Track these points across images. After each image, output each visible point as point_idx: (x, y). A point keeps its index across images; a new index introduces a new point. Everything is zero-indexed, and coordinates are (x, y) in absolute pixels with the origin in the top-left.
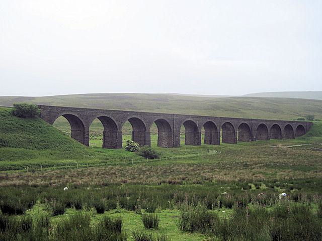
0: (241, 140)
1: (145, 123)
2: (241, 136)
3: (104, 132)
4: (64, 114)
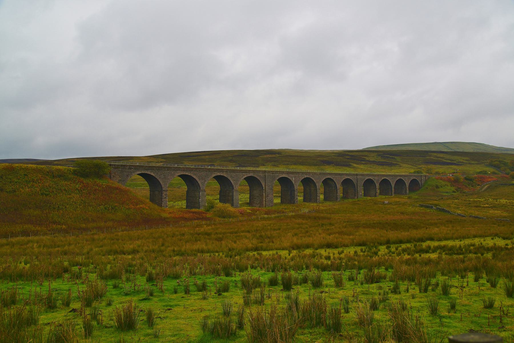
0: (345, 197)
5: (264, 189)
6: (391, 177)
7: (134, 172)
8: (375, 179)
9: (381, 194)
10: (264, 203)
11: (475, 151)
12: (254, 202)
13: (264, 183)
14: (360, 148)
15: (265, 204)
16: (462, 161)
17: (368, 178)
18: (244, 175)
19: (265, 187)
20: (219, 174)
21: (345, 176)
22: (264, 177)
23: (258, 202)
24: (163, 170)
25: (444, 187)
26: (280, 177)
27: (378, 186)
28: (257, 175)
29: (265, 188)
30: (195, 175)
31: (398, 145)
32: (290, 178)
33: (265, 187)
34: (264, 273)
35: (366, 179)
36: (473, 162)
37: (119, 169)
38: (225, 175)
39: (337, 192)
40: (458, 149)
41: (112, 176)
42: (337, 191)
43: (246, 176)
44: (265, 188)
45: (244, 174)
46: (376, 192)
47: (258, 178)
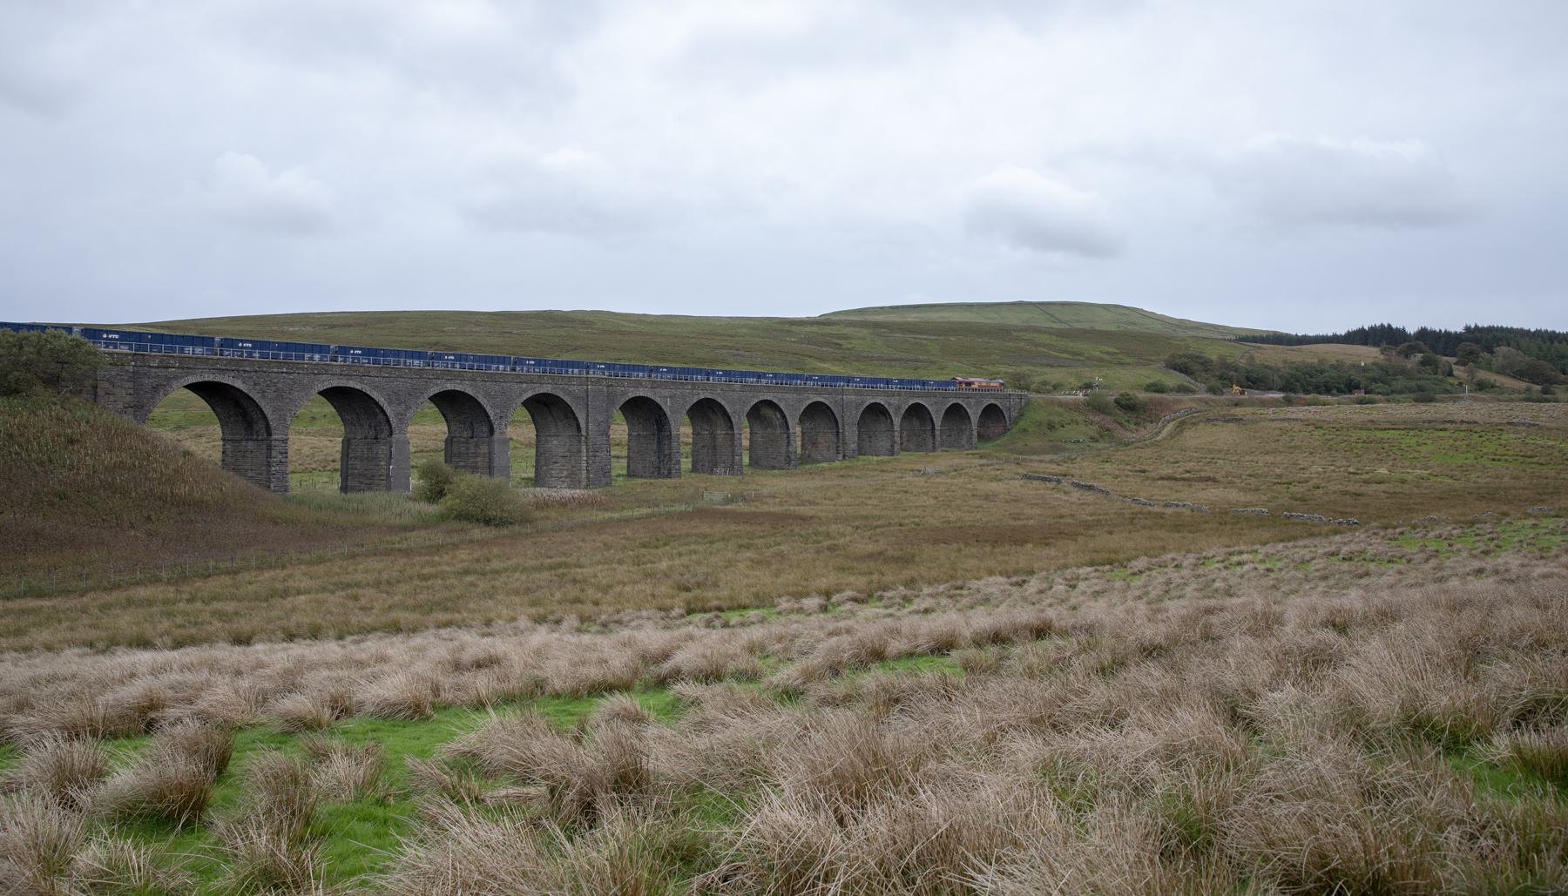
1: (488, 409)
2: (809, 441)
3: (449, 442)
4: (192, 380)
5: (584, 433)
6: (934, 399)
7: (176, 378)
8: (890, 405)
9: (755, 463)
10: (584, 476)
11: (1121, 329)
12: (551, 474)
13: (584, 416)
14: (814, 312)
15: (588, 478)
16: (1097, 354)
17: (873, 401)
18: (525, 391)
19: (587, 423)
20: (449, 386)
21: (811, 396)
22: (584, 395)
23: (565, 473)
24: (275, 370)
25: (1069, 427)
26: (631, 395)
27: (897, 421)
28: (563, 389)
29: (587, 429)
30: (375, 388)
31: (903, 307)
32: (658, 400)
33: (587, 423)
34: (1161, 601)
35: (867, 404)
36: (1129, 360)
37: (127, 368)
38: (469, 391)
39: (789, 442)
40: (1078, 321)
41: (100, 392)
42: (788, 437)
43: (530, 394)
44: (587, 429)
45: (525, 385)
46: (894, 442)
47: (567, 399)
